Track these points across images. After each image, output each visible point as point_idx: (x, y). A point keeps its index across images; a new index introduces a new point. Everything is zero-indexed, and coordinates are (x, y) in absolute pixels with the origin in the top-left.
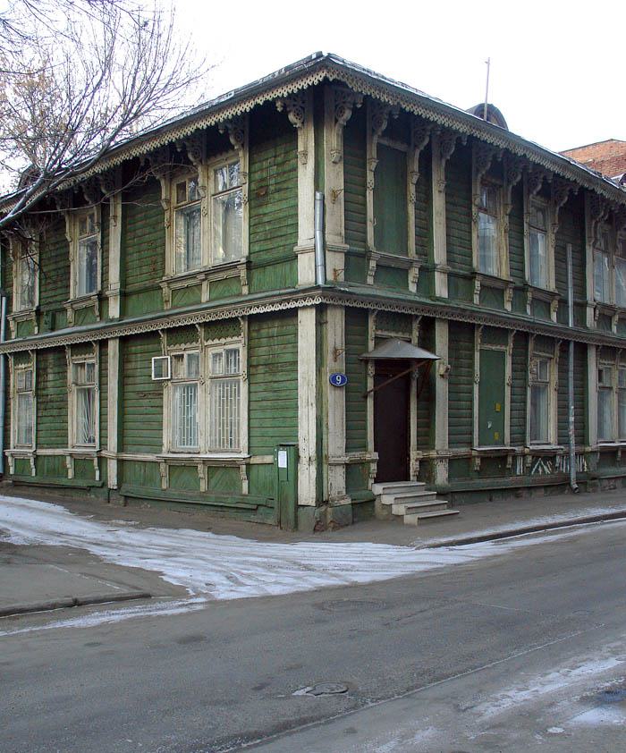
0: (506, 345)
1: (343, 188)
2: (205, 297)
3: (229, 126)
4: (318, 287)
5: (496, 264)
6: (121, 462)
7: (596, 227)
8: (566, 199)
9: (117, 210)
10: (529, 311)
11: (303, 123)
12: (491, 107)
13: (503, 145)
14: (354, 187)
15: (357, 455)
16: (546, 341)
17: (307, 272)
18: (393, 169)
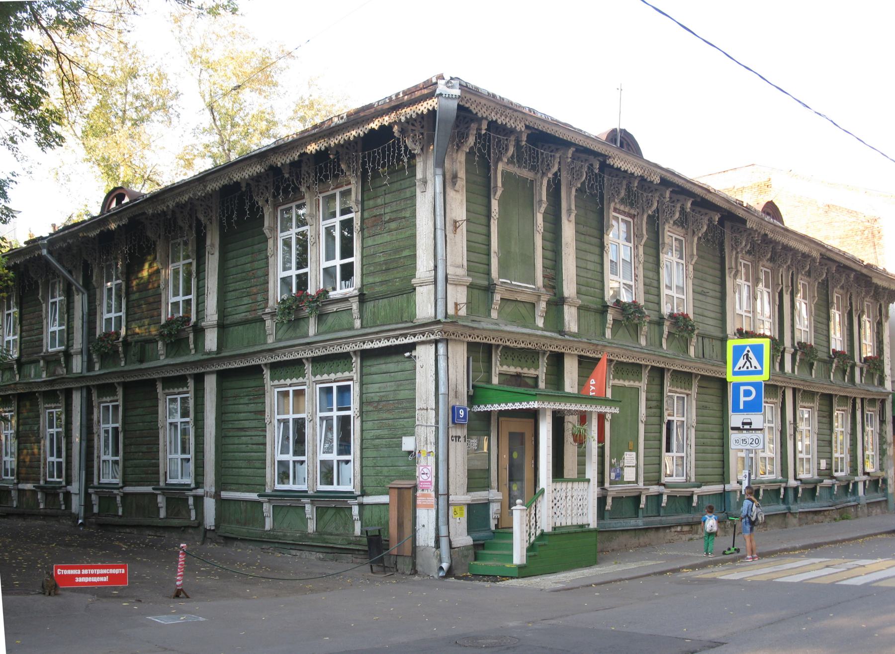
0: (640, 380)
1: (465, 218)
2: (312, 331)
3: (340, 150)
4: (438, 322)
5: (620, 285)
6: (221, 502)
7: (737, 258)
8: (705, 228)
9: (213, 240)
10: (664, 346)
11: (422, 149)
12: (624, 132)
13: (638, 172)
14: (479, 215)
15: (479, 496)
16: (684, 377)
17: (424, 306)
18: (520, 193)
